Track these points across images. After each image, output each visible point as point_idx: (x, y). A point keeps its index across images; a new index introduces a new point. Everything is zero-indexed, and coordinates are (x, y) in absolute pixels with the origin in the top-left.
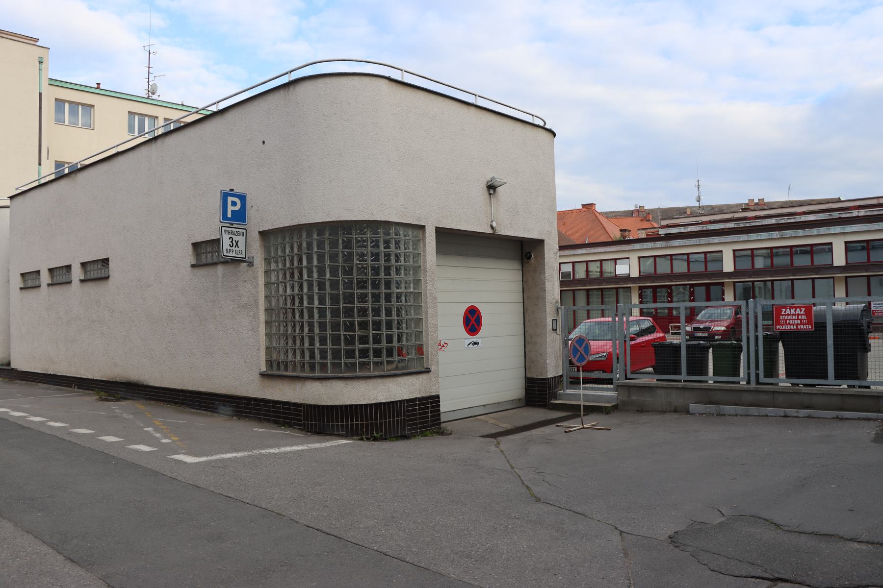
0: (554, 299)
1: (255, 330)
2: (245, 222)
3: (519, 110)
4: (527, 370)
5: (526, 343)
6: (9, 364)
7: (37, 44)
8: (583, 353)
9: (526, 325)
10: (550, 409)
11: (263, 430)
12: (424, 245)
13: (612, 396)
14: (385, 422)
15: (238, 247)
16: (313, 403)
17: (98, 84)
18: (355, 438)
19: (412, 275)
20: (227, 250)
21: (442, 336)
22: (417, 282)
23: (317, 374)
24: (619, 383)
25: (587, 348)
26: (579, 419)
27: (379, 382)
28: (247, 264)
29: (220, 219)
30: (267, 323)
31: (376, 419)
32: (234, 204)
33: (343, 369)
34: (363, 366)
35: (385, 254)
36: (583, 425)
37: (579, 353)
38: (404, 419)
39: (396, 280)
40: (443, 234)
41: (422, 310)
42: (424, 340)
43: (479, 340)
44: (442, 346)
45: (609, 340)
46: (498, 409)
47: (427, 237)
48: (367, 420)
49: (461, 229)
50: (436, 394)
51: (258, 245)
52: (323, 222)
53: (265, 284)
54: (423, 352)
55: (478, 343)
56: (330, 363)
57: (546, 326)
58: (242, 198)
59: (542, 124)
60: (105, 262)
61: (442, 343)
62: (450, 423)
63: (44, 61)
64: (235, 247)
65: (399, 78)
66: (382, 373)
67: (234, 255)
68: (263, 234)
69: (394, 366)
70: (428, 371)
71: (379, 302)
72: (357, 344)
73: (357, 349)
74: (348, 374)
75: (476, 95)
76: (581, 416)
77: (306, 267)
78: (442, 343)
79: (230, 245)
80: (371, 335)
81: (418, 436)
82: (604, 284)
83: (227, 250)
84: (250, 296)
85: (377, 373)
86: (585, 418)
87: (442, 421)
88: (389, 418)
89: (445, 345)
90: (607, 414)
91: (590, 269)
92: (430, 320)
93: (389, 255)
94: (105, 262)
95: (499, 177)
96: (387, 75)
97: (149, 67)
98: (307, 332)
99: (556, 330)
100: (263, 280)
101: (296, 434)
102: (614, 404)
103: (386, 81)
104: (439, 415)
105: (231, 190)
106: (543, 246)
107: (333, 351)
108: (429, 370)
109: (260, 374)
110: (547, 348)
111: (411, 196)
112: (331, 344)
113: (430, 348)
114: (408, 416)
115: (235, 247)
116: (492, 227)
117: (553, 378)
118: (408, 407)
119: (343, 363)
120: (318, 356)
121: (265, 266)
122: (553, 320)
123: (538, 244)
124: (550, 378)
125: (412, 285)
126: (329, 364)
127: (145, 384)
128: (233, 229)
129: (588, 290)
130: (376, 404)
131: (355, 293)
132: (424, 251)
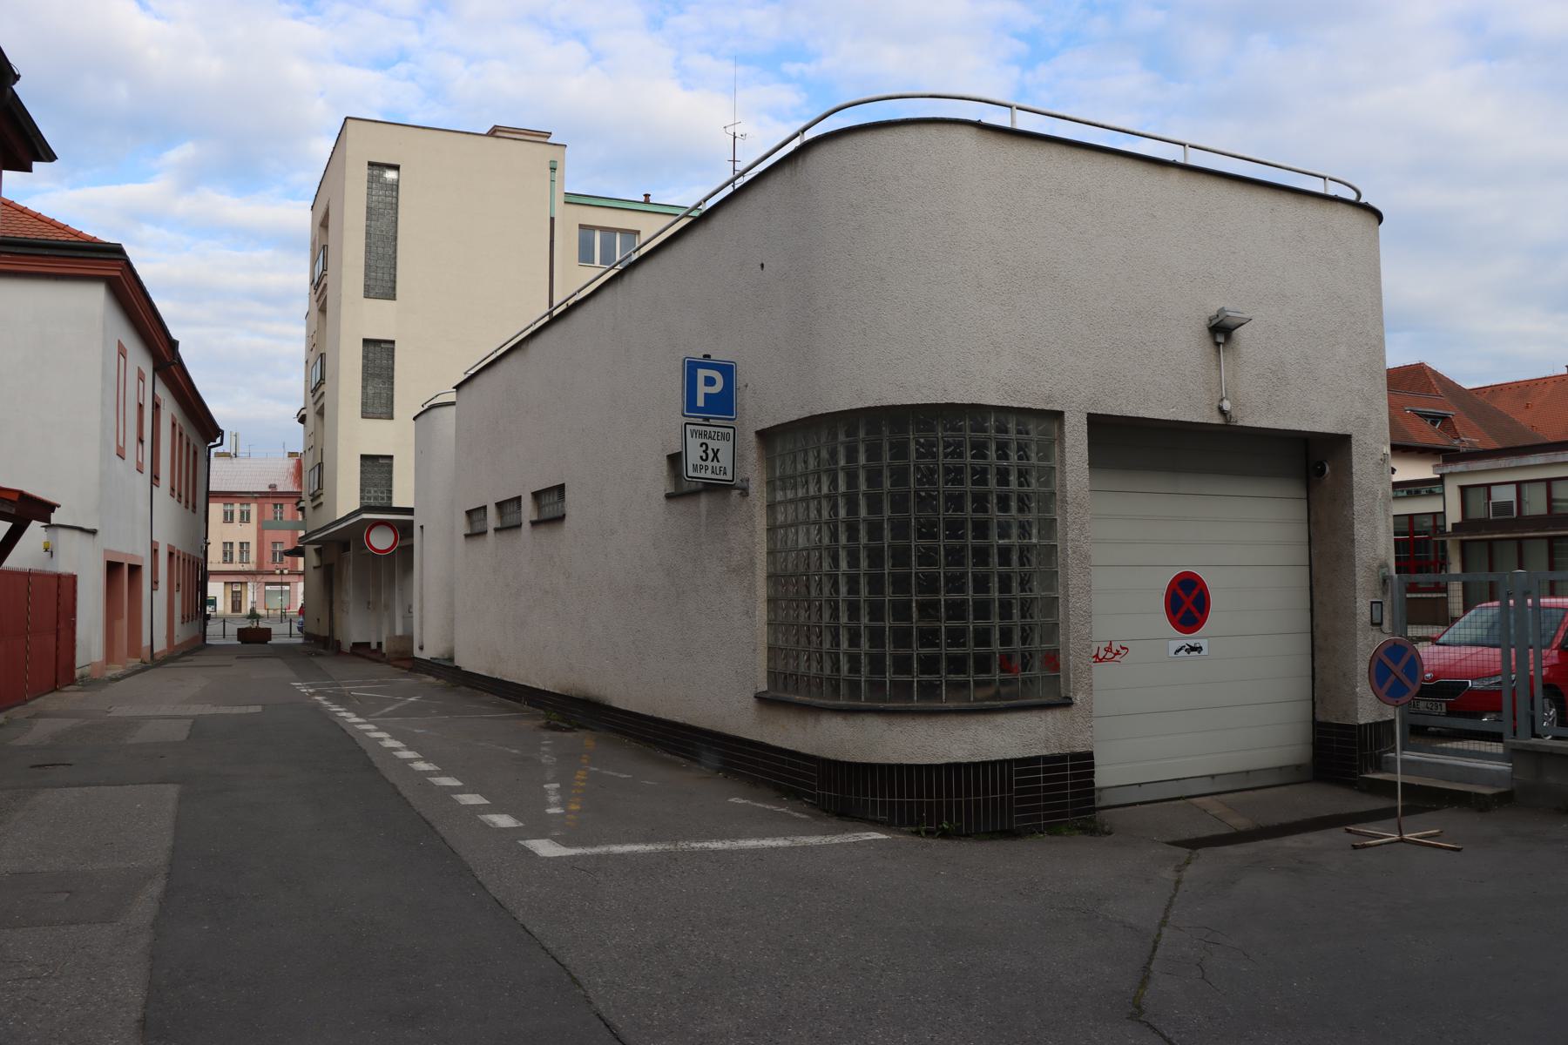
0: (1374, 559)
1: (749, 613)
2: (733, 415)
3: (1290, 169)
4: (1317, 706)
5: (1316, 649)
6: (451, 659)
7: (549, 141)
8: (1403, 677)
9: (1315, 613)
10: (1362, 791)
11: (745, 801)
12: (1062, 451)
13: (1498, 772)
14: (968, 803)
15: (718, 461)
16: (831, 756)
17: (647, 196)
18: (906, 829)
19: (1035, 511)
20: (695, 468)
21: (1104, 631)
22: (1049, 526)
23: (842, 702)
24: (1514, 744)
25: (1415, 663)
26: (1393, 822)
27: (955, 721)
28: (738, 492)
29: (683, 411)
30: (770, 600)
31: (949, 795)
32: (710, 381)
33: (888, 693)
34: (929, 690)
35: (973, 469)
36: (1401, 834)
37: (1393, 677)
38: (1010, 798)
39: (998, 522)
40: (1100, 426)
41: (1057, 581)
42: (1061, 639)
43: (1203, 643)
44: (1112, 654)
45: (1494, 646)
46: (1244, 783)
47: (1067, 434)
48: (930, 795)
49: (1146, 416)
50: (1084, 749)
51: (755, 455)
52: (851, 410)
53: (767, 529)
54: (1058, 665)
55: (1201, 648)
56: (865, 681)
57: (1355, 614)
58: (727, 370)
59: (1352, 196)
60: (561, 489)
61: (1115, 647)
62: (1130, 808)
63: (559, 166)
64: (713, 461)
65: (1006, 123)
66: (964, 705)
67: (709, 475)
68: (765, 436)
69: (991, 691)
70: (1067, 703)
71: (987, 565)
72: (915, 646)
73: (915, 656)
74: (896, 705)
75: (1184, 145)
76: (1396, 816)
77: (844, 495)
78: (1115, 647)
79: (701, 457)
80: (943, 628)
81: (1041, 833)
82: (1483, 531)
83: (695, 468)
84: (743, 550)
85: (951, 705)
86: (1407, 821)
87: (1098, 804)
88: (977, 794)
89: (1123, 652)
90: (1481, 810)
91: (1555, 496)
92: (1072, 600)
93: (984, 471)
94: (561, 489)
95: (1234, 308)
96: (974, 118)
97: (734, 161)
98: (827, 620)
99: (1380, 624)
100: (764, 521)
101: (797, 814)
102: (1503, 790)
103: (973, 130)
104: (1092, 792)
105: (705, 356)
106: (1350, 448)
107: (896, 659)
108: (1068, 701)
109: (755, 697)
110: (1356, 661)
111: (1030, 353)
112: (892, 646)
113: (1074, 654)
114: (1019, 792)
115: (713, 461)
116: (1222, 411)
117: (1370, 724)
118: (1019, 773)
119: (888, 682)
120: (845, 667)
121: (767, 494)
122: (1372, 603)
123: (1339, 444)
124: (1365, 725)
125: (1034, 531)
126: (863, 684)
127: (606, 703)
128: (708, 429)
129: (1551, 539)
130: (948, 766)
131: (913, 547)
132: (1063, 462)
